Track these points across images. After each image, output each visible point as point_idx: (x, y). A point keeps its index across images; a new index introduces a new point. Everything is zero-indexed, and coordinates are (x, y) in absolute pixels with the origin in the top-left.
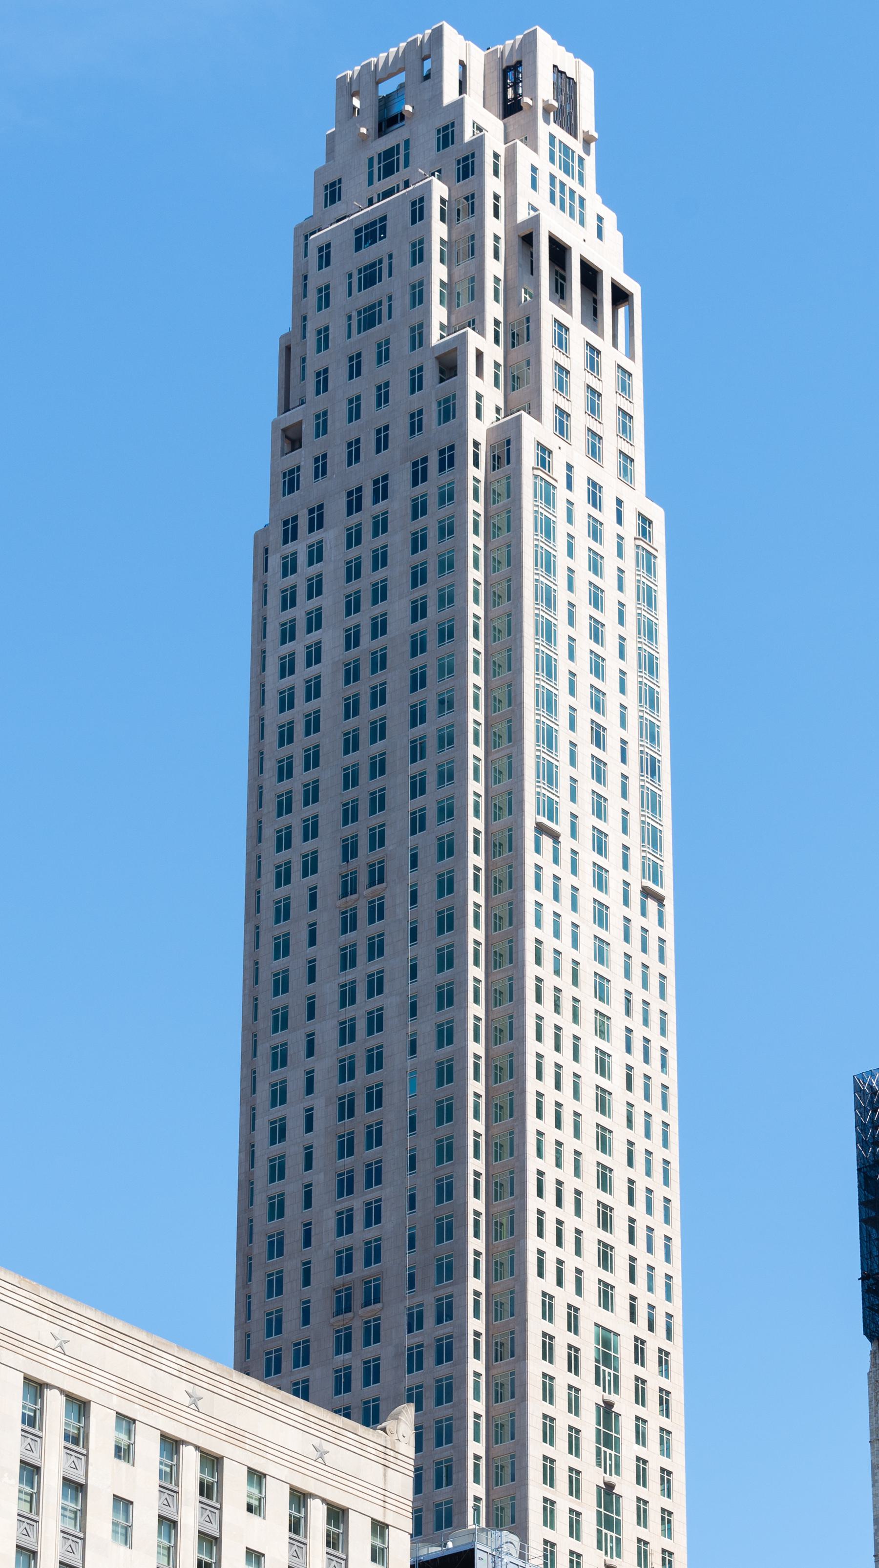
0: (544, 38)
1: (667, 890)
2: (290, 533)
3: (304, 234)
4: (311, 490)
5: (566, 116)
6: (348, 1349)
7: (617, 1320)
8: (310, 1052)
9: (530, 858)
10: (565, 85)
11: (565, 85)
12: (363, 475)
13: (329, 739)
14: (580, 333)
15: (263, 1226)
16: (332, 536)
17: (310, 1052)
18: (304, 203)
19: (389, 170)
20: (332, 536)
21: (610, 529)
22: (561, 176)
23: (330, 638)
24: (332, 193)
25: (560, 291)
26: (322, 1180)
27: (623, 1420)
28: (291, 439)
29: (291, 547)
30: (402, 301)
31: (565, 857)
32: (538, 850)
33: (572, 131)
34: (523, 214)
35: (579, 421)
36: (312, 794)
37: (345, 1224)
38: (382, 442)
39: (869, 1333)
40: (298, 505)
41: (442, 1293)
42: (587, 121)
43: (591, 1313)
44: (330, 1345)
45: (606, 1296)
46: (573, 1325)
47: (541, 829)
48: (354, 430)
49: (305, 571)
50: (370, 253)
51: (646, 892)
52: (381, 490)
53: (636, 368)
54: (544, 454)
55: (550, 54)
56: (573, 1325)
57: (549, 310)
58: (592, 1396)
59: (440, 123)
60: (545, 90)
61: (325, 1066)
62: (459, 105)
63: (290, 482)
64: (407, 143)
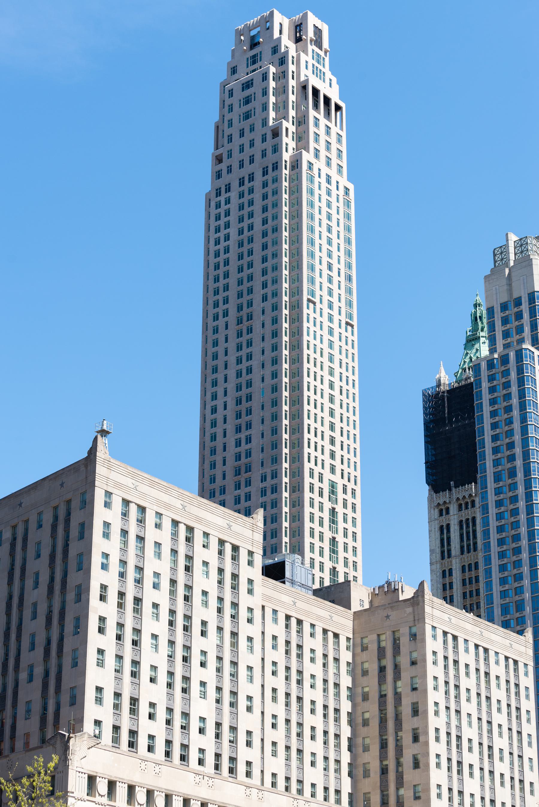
0: (310, 15)
1: (355, 323)
2: (218, 193)
3: (223, 86)
4: (226, 178)
5: (318, 43)
6: (239, 489)
7: (337, 478)
8: (226, 381)
9: (305, 311)
10: (318, 31)
11: (318, 31)
12: (245, 172)
13: (233, 268)
14: (323, 121)
15: (209, 444)
16: (233, 195)
17: (226, 381)
18: (223, 74)
19: (254, 62)
20: (233, 195)
21: (334, 192)
22: (316, 64)
23: (233, 231)
24: (234, 71)
25: (316, 106)
26: (230, 427)
27: (339, 514)
28: (219, 159)
29: (219, 198)
30: (259, 110)
31: (318, 310)
32: (308, 308)
33: (320, 48)
34: (303, 78)
35: (323, 153)
36: (226, 301)
37: (238, 443)
38: (252, 161)
39: (428, 483)
40: (222, 183)
41: (273, 468)
42: (326, 44)
43: (327, 475)
44: (233, 487)
45: (333, 470)
46: (321, 480)
47: (309, 300)
48: (241, 156)
49: (224, 207)
50: (247, 92)
51: (347, 323)
52: (251, 178)
53: (344, 134)
54: (310, 165)
55: (312, 20)
56: (321, 480)
57: (312, 113)
58: (328, 505)
59: (273, 46)
60: (311, 33)
61: (231, 386)
62: (279, 39)
63: (218, 175)
64: (261, 52)
